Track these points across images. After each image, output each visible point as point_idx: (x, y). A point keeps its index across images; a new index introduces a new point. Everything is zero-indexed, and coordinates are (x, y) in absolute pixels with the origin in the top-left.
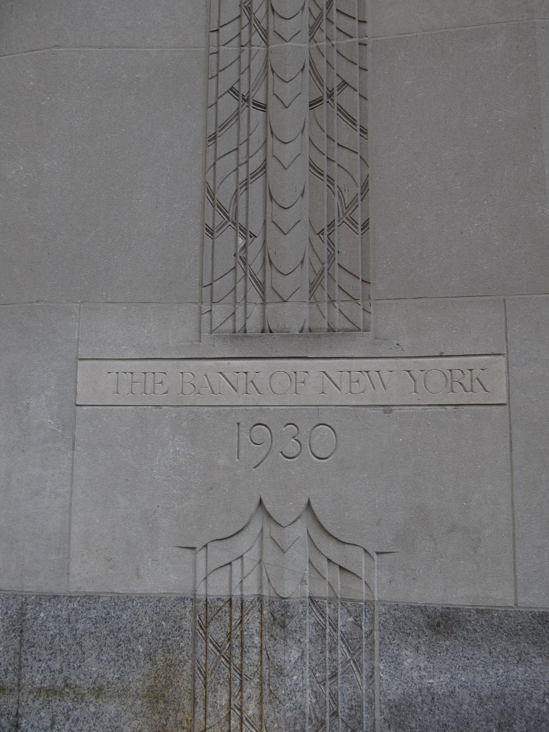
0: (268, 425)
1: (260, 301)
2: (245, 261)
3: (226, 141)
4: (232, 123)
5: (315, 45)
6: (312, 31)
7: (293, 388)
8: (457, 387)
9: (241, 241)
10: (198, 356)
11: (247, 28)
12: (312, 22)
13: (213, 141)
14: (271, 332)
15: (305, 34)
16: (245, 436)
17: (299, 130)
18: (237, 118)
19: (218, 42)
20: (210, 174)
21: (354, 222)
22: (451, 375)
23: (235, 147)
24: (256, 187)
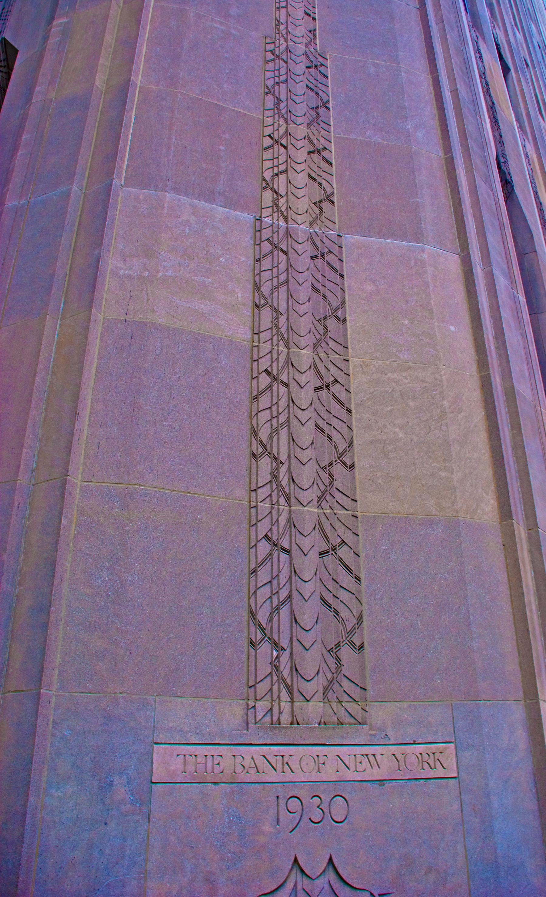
0: (300, 797)
1: (289, 700)
2: (277, 668)
3: (263, 576)
4: (267, 561)
5: (322, 511)
6: (320, 499)
7: (317, 768)
8: (426, 766)
9: (275, 653)
10: (247, 742)
11: (276, 492)
12: (319, 494)
13: (254, 574)
14: (298, 724)
15: (315, 502)
16: (282, 803)
17: (314, 573)
18: (270, 557)
19: (257, 498)
20: (252, 600)
21: (354, 645)
22: (422, 757)
23: (269, 580)
24: (285, 612)
